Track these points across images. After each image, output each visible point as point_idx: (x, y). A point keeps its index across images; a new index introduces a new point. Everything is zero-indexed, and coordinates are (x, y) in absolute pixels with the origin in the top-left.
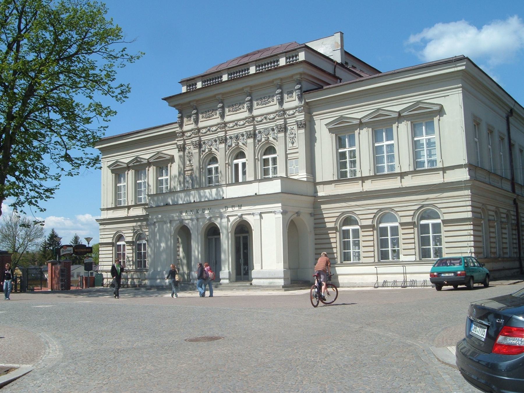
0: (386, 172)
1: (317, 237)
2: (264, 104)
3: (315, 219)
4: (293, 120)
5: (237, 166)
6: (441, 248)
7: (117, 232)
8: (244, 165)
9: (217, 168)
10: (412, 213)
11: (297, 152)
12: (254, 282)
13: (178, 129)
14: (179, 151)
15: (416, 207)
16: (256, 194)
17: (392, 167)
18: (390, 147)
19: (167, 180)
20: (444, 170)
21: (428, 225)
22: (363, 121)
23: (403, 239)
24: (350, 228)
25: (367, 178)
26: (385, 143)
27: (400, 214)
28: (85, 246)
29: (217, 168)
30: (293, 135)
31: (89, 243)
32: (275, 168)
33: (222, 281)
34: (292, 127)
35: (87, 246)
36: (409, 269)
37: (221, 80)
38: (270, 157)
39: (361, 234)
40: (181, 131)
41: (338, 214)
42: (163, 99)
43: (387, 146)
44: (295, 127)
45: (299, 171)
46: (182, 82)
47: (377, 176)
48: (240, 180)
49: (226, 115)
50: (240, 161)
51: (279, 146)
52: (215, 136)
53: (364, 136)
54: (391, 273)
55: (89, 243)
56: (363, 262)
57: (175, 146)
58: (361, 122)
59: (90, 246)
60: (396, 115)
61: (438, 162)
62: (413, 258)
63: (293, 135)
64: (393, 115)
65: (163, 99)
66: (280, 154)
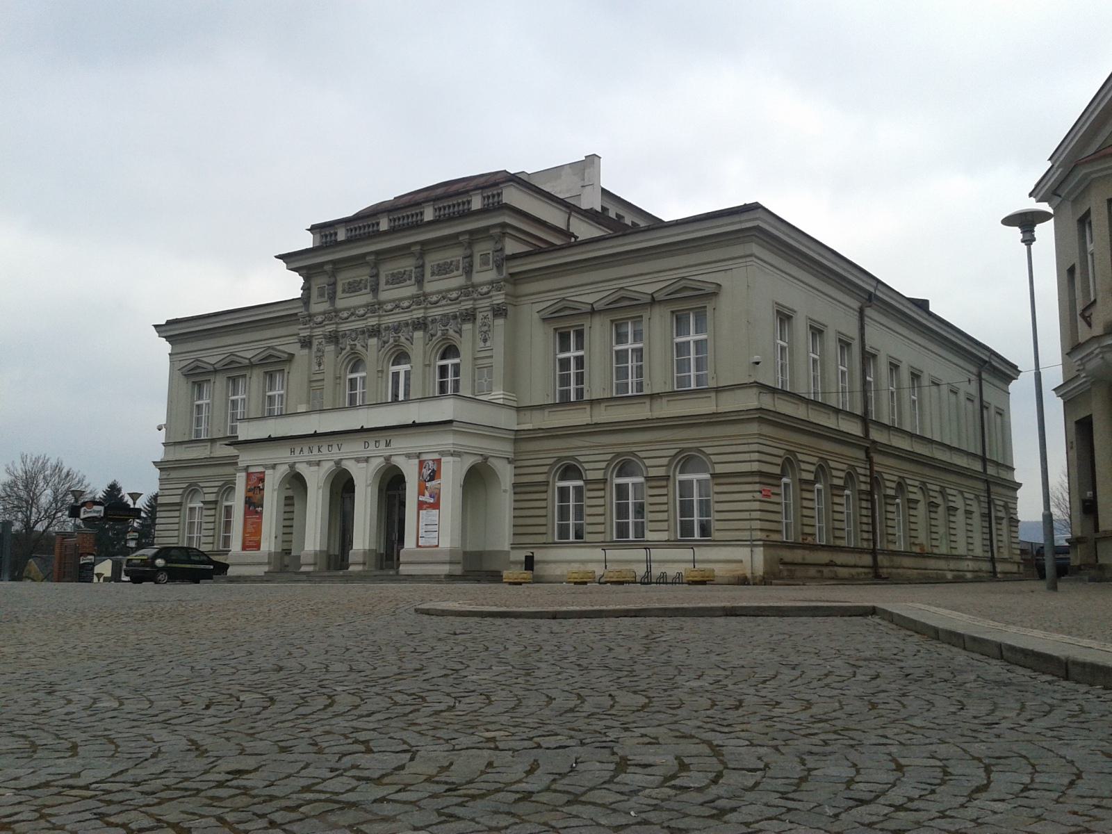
0: (693, 387)
1: (518, 497)
2: (353, 292)
3: (515, 467)
4: (485, 303)
5: (396, 375)
6: (710, 521)
7: (191, 485)
8: (407, 373)
9: (457, 366)
10: (603, 465)
11: (491, 357)
12: (404, 569)
13: (302, 310)
14: (302, 347)
15: (673, 452)
16: (414, 422)
17: (640, 386)
18: (639, 353)
19: (282, 396)
20: (718, 390)
21: (692, 481)
22: (658, 297)
23: (651, 504)
24: (571, 484)
25: (599, 401)
26: (692, 337)
27: (648, 462)
28: (129, 505)
29: (457, 366)
30: (486, 328)
31: (134, 504)
32: (457, 383)
33: (351, 568)
34: (485, 314)
35: (132, 506)
36: (656, 554)
37: (422, 220)
38: (449, 362)
39: (587, 494)
40: (306, 313)
41: (551, 461)
42: (276, 257)
43: (696, 342)
44: (490, 315)
45: (494, 388)
46: (313, 229)
47: (621, 399)
48: (401, 397)
49: (426, 281)
50: (402, 368)
51: (465, 347)
52: (360, 325)
53: (598, 332)
54: (631, 559)
55: (134, 504)
56: (587, 540)
57: (294, 339)
58: (593, 308)
59: (137, 506)
60: (648, 299)
61: (710, 377)
62: (664, 536)
63: (486, 328)
64: (707, 289)
65: (276, 257)
66: (465, 359)
